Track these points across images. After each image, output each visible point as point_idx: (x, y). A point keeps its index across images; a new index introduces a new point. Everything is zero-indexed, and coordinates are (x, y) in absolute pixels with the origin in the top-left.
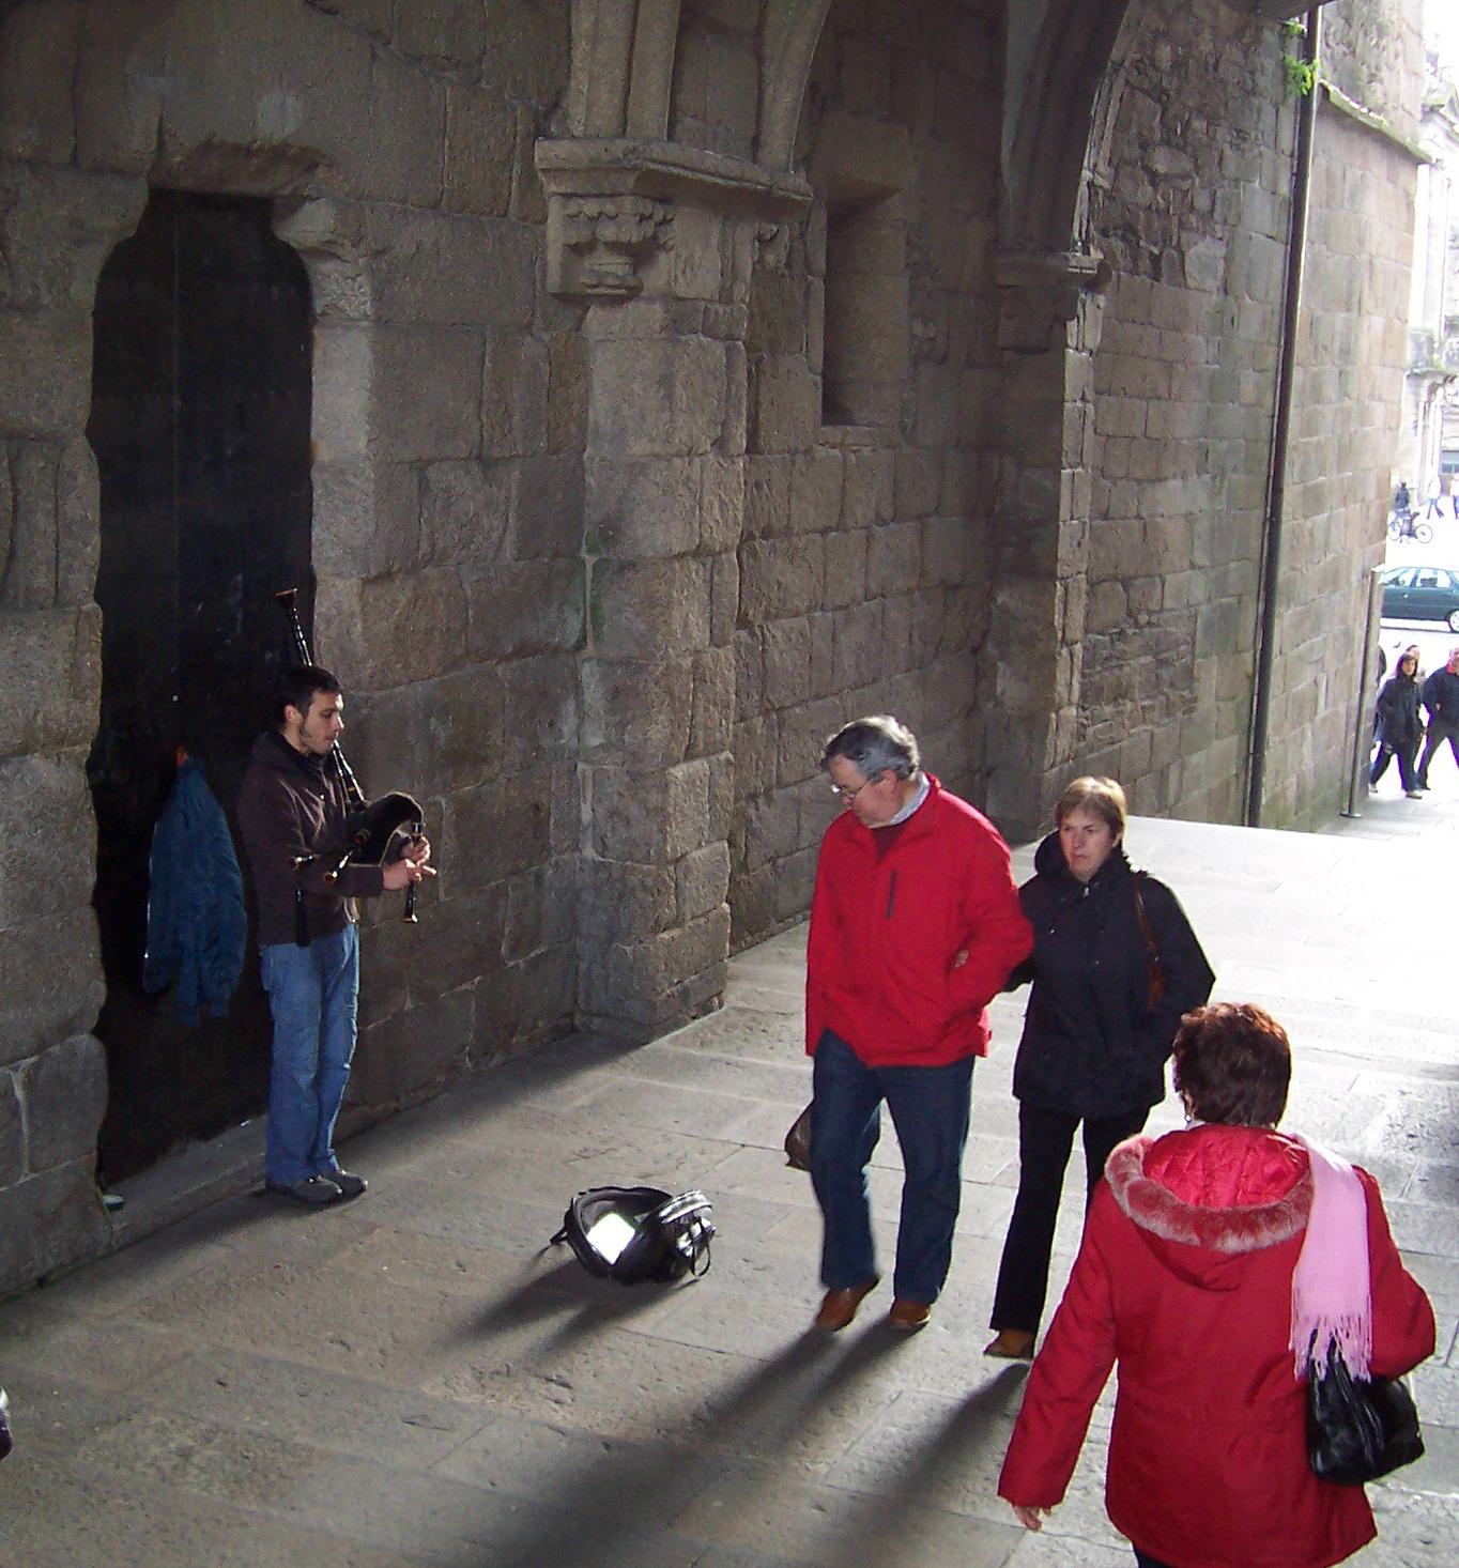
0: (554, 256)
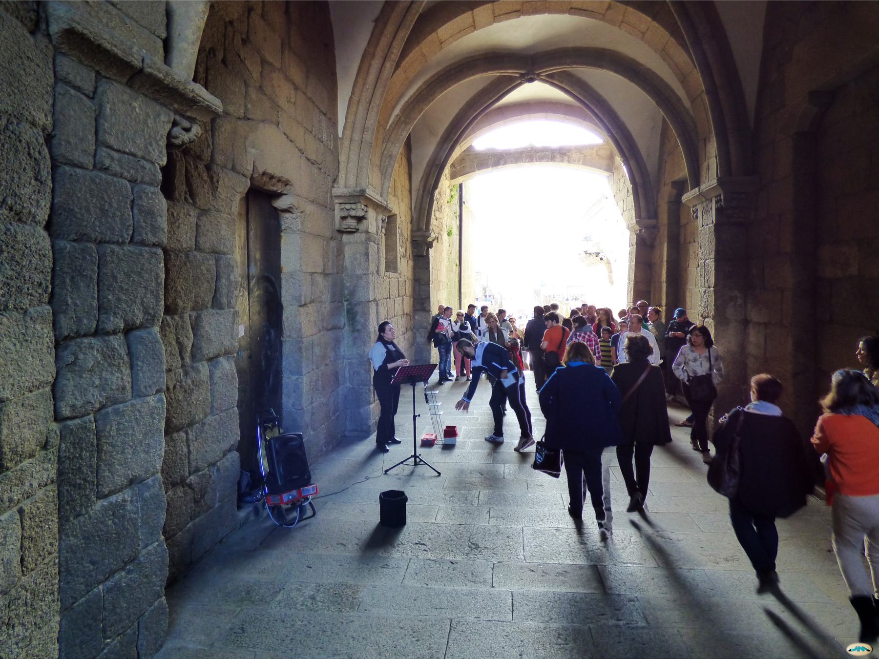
0: (337, 219)
